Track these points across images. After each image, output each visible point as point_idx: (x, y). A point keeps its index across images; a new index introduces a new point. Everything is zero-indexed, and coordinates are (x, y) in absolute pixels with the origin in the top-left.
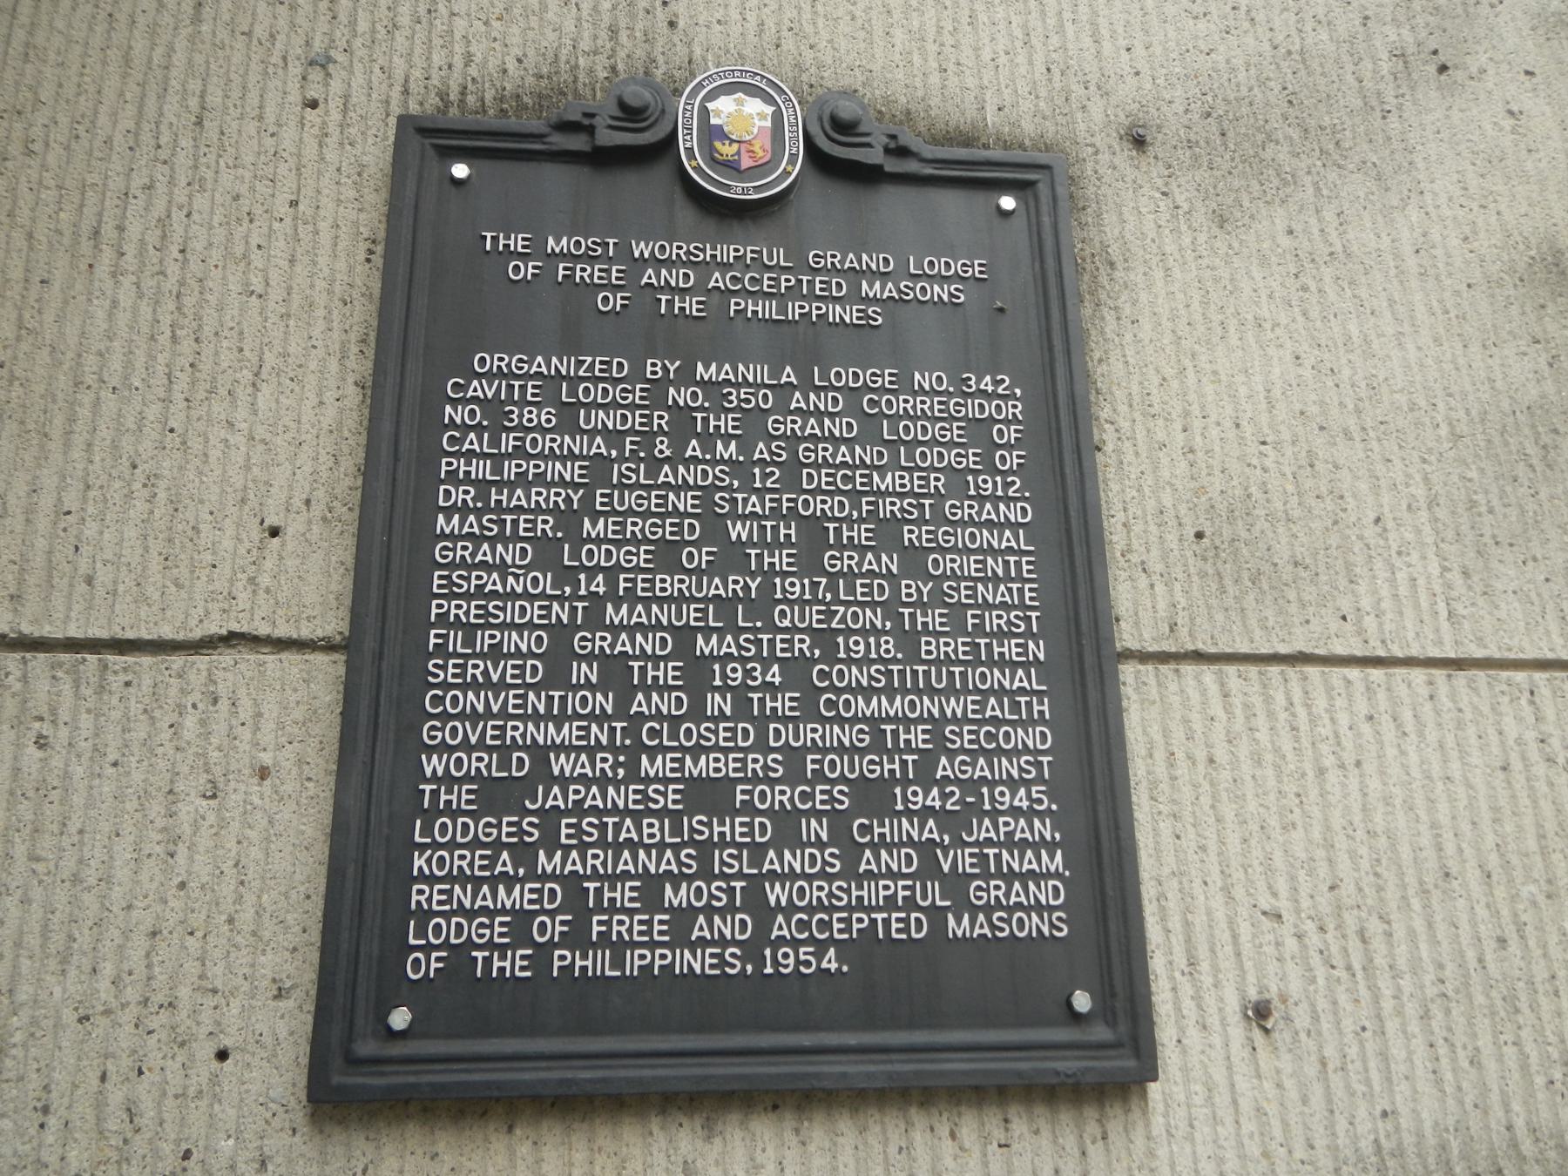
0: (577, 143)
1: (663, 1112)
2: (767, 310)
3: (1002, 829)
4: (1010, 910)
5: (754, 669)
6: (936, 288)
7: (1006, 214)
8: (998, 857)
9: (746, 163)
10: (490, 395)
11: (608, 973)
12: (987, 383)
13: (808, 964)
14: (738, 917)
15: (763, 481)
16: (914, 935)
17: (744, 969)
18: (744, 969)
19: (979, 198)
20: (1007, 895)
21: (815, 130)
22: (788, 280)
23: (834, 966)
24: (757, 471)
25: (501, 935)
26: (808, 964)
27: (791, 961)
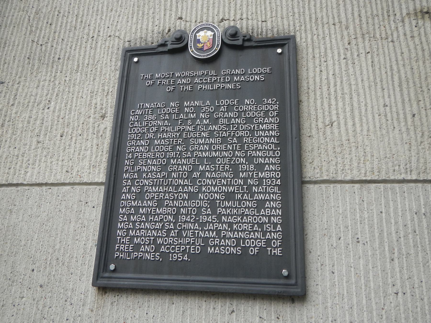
1: (283, 299)
2: (209, 87)
4: (225, 246)
5: (274, 181)
6: (256, 77)
7: (280, 54)
8: (198, 233)
9: (205, 48)
10: (141, 113)
11: (127, 258)
12: (270, 101)
13: (180, 258)
14: (151, 246)
17: (160, 259)
18: (160, 259)
19: (269, 51)
20: (220, 243)
21: (224, 37)
22: (214, 79)
23: (186, 259)
25: (264, 245)
26: (180, 258)
27: (176, 257)
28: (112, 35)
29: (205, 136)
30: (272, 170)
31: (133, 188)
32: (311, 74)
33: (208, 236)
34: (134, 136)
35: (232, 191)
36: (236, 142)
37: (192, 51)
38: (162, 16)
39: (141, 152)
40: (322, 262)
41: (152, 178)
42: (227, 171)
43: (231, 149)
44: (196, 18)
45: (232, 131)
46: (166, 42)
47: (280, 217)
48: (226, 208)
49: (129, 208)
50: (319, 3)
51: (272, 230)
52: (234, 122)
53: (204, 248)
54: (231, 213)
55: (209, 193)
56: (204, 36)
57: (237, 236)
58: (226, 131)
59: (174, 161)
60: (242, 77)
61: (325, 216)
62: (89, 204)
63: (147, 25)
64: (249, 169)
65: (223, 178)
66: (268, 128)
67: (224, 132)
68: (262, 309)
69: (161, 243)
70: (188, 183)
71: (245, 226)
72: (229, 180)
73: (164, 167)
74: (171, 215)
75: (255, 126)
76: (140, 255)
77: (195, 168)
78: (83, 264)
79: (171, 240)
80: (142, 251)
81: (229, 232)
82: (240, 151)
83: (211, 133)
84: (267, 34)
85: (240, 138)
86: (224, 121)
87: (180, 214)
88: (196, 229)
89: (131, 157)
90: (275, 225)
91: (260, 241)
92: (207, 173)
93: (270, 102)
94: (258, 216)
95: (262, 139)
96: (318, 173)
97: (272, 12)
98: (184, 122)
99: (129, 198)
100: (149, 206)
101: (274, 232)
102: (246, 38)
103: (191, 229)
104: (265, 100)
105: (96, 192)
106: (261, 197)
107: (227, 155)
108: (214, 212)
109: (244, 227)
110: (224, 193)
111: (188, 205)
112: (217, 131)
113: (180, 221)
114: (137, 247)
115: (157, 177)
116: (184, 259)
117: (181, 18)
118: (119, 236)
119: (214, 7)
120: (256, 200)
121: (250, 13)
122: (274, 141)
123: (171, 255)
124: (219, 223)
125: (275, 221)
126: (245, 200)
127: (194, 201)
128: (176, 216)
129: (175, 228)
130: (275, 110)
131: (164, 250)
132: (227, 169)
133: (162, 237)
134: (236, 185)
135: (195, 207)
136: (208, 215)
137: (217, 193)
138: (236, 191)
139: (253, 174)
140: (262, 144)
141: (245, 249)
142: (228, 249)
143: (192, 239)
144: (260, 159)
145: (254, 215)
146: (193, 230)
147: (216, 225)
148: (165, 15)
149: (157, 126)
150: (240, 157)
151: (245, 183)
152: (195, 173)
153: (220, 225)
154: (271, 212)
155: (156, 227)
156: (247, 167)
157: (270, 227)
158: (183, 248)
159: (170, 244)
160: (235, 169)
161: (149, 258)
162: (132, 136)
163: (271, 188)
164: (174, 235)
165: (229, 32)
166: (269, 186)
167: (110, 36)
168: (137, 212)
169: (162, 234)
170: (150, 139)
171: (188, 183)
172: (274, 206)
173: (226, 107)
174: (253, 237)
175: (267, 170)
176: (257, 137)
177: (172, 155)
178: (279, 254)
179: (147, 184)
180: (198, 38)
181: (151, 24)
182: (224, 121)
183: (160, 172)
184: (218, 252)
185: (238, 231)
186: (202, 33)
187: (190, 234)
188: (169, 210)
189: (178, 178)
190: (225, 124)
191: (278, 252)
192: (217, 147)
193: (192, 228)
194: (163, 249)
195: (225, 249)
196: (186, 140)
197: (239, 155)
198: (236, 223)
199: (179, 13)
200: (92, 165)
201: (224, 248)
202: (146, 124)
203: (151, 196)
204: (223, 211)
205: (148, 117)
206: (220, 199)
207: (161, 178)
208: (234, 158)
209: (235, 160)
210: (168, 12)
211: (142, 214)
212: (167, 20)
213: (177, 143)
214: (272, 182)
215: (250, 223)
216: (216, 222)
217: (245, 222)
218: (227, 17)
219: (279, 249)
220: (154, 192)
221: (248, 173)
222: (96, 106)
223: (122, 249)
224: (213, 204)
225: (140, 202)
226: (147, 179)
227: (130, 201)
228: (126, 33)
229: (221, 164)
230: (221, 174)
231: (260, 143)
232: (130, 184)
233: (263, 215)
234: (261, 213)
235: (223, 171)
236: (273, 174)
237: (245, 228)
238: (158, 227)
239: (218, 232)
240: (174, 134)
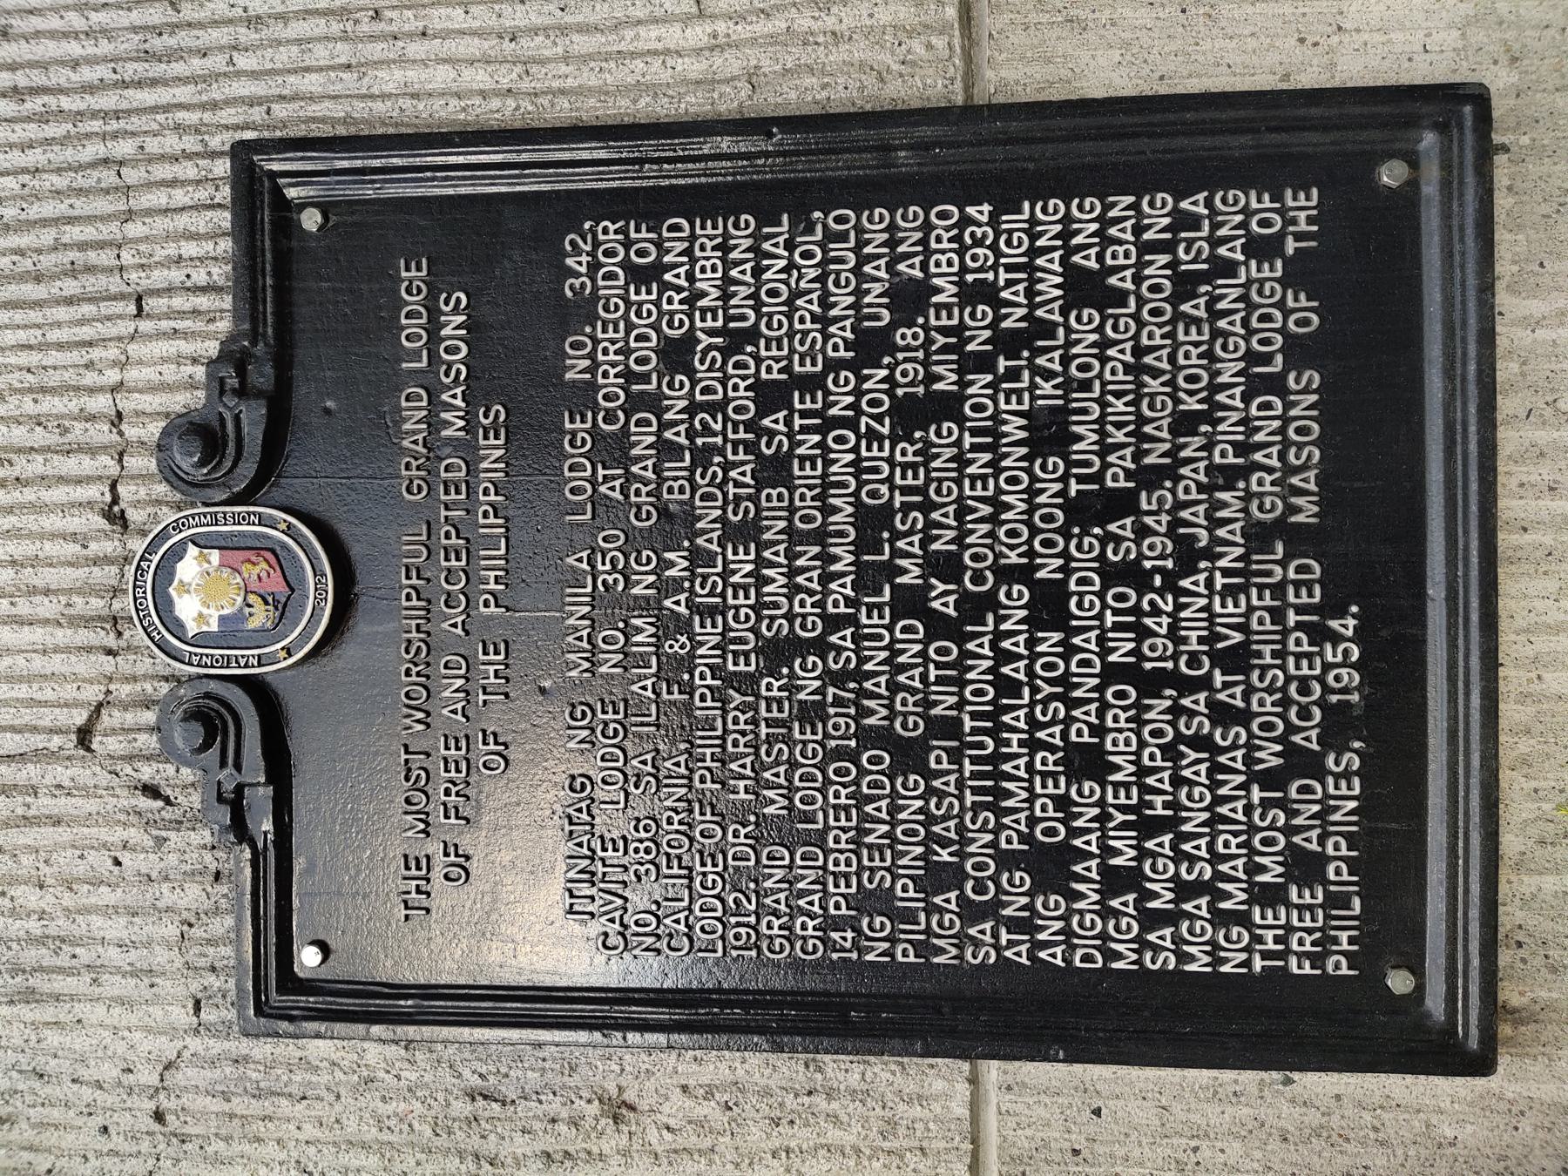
0: (261, 795)
3: (1194, 496)
4: (1286, 444)
5: (972, 234)
8: (1226, 573)
9: (277, 585)
13: (1346, 652)
15: (715, 435)
16: (1317, 575)
23: (1351, 622)
24: (699, 441)
27: (1344, 671)
28: (152, 1105)
29: (749, 567)
30: (924, 242)
31: (1007, 912)
32: (442, 76)
33: (1237, 526)
34: (738, 924)
35: (1023, 422)
36: (781, 415)
37: (276, 660)
38: (63, 834)
39: (824, 884)
40: (1329, 30)
41: (960, 817)
42: (927, 455)
43: (816, 438)
44: (89, 650)
45: (725, 440)
46: (220, 799)
47: (1146, 199)
48: (1105, 450)
49: (1112, 923)
50: (64, 43)
51: (1204, 234)
52: (682, 428)
53: (1298, 540)
54: (1127, 423)
55: (1034, 530)
56: (202, 594)
57: (1238, 391)
58: (727, 466)
59: (872, 712)
60: (444, 397)
61: (1128, 12)
62: (1079, 1142)
63: (109, 911)
64: (916, 349)
65: (960, 470)
66: (714, 269)
67: (733, 474)
68: (1540, 280)
69: (1279, 748)
70: (983, 634)
71: (1187, 356)
72: (968, 440)
73: (909, 757)
74: (1141, 708)
75: (702, 330)
76: (1335, 847)
77: (910, 603)
78: (1381, 1136)
79: (1261, 703)
80: (1322, 841)
81: (1220, 428)
82: (827, 393)
83: (735, 534)
85: (770, 396)
86: (676, 479)
87: (1136, 667)
88: (1209, 583)
89: (849, 935)
90: (1184, 222)
91: (1255, 286)
92: (935, 546)
93: (584, 259)
94: (1141, 302)
95: (773, 293)
96: (929, 46)
97: (90, 269)
98: (675, 670)
99: (1058, 925)
100: (1103, 818)
101: (1215, 226)
102: (233, 382)
103: (1207, 608)
104: (572, 287)
105: (1020, 1108)
106: (1050, 286)
107: (850, 457)
108: (1124, 504)
109: (1191, 360)
110: (1032, 463)
111: (1091, 628)
112: (724, 509)
113: (1170, 665)
114: (1304, 867)
115: (952, 789)
116: (1350, 633)
117: (84, 736)
118: (1247, 964)
119: (35, 562)
120: (1064, 312)
121: (90, 378)
122: (781, 240)
123: (1334, 698)
124: (1177, 478)
125: (1166, 221)
126: (1066, 361)
127: (1074, 599)
128: (1151, 684)
129: (1205, 683)
130: (627, 235)
131: (1314, 734)
132: (915, 454)
133: (1250, 748)
134: (996, 403)
135: (1101, 595)
136: (1142, 532)
137: (1032, 493)
138: (1026, 407)
139: (944, 331)
140: (796, 294)
141: (1298, 351)
142: (1298, 431)
143: (1255, 602)
144: (867, 300)
145: (1136, 316)
146: (1210, 597)
147: (1187, 490)
148: (57, 823)
149: (691, 811)
150: (858, 393)
151: (983, 363)
152: (936, 605)
153: (1184, 471)
154: (1120, 242)
155: (1203, 780)
156: (906, 360)
157: (1190, 243)
159: (1285, 702)
160: (916, 413)
161: (1352, 804)
162: (737, 937)
163: (1009, 243)
164: (1238, 690)
165: (187, 462)
166: (998, 254)
167: (159, 1116)
168: (1130, 880)
169: (1234, 746)
170: (757, 842)
171: (983, 634)
172: (1094, 227)
173: (601, 472)
174: (1238, 317)
175: (924, 267)
176: (759, 316)
177: (842, 720)
178: (1314, 203)
179: (989, 837)
180: (214, 627)
181: (106, 896)
182: (676, 479)
183: (929, 775)
185: (1214, 388)
186: (187, 608)
187: (1229, 610)
188: (1116, 718)
189: (962, 683)
190: (693, 473)
191: (1304, 205)
192: (806, 503)
193: (1203, 602)
194: (1309, 739)
195: (1300, 446)
196: (779, 653)
197: (850, 399)
198: (1177, 401)
199: (56, 741)
200: (879, 1142)
201: (1293, 450)
203: (1051, 814)
204: (1122, 461)
206: (1064, 479)
207: (960, 771)
208: (864, 419)
209: (871, 416)
210: (45, 804)
211: (1142, 854)
212: (91, 805)
213: (779, 701)
214: (978, 242)
215: (1171, 335)
216: (1173, 492)
217: (1172, 359)
218: (97, 493)
219: (1291, 203)
220: (1031, 800)
221: (937, 352)
222: (558, 1157)
223: (1313, 944)
224: (1093, 509)
225: (1078, 868)
226: (964, 841)
227: (1075, 919)
228: (148, 1030)
229: (890, 480)
230: (940, 481)
231: (789, 302)
232: (988, 926)
233: (1138, 279)
234: (1129, 285)
235: (927, 472)
236: (939, 240)
237: (1199, 356)
238: (1203, 767)
239: (1227, 477)
240: (736, 721)
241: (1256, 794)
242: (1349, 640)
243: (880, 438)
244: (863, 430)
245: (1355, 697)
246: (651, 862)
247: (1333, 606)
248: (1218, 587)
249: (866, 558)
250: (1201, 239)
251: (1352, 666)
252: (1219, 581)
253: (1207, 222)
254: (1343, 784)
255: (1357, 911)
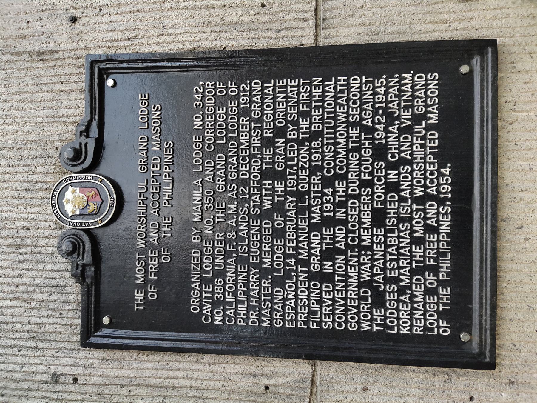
3: (393, 99)
4: (427, 97)
8: (405, 101)
10: (210, 306)
13: (447, 180)
16: (436, 137)
17: (449, 205)
18: (449, 205)
21: (79, 168)
23: (448, 170)
27: (446, 186)
84: (81, 91)
95: (268, 106)
116: (448, 173)
158: (430, 159)
184: (435, 107)
186: (69, 209)
202: (230, 297)
205: (219, 293)
208: (300, 163)
241: (414, 207)
242: (448, 176)
243: (305, 168)
244: (300, 166)
245: (449, 196)
246: (222, 293)
247: (442, 165)
248: (402, 106)
249: (300, 204)
250: (407, 206)
251: (449, 185)
252: (403, 104)
253: (410, 200)
254: (445, 217)
255: (449, 258)
